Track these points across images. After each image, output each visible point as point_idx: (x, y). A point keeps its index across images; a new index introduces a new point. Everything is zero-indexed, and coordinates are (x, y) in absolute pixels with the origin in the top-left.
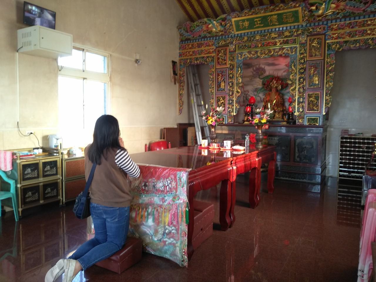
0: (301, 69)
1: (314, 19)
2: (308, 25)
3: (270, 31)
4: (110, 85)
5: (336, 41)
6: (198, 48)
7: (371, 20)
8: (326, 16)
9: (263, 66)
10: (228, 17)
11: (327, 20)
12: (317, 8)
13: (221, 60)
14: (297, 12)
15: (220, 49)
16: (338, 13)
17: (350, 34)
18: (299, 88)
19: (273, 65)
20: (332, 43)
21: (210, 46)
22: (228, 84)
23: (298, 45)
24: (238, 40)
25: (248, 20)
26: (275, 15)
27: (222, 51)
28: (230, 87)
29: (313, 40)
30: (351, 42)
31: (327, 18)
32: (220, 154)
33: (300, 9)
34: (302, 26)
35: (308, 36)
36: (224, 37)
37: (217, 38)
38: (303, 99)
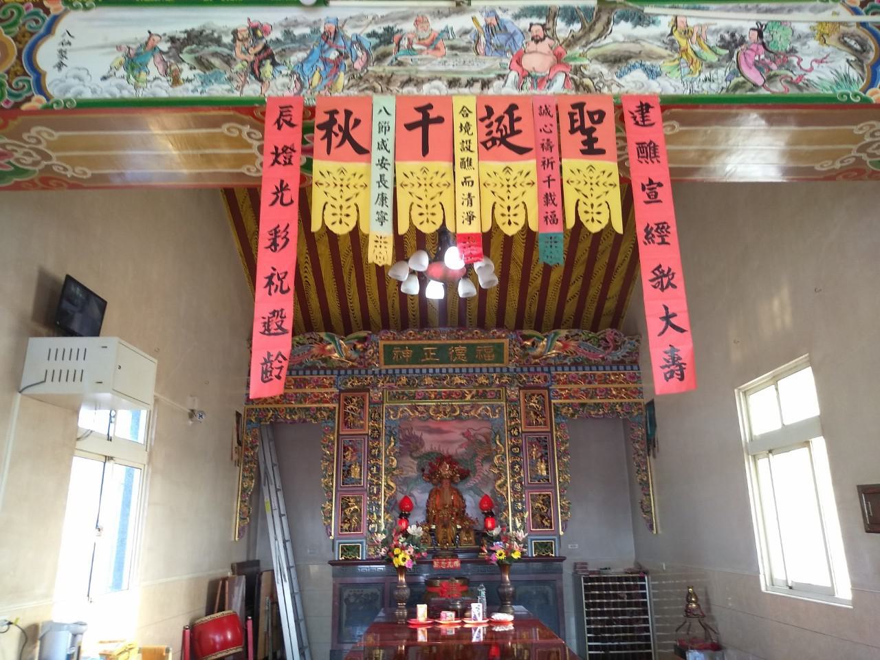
0: (515, 446)
1: (527, 361)
2: (519, 369)
3: (451, 371)
4: (148, 472)
5: (567, 401)
6: (297, 388)
7: (615, 374)
8: (545, 359)
9: (418, 434)
10: (374, 337)
11: (549, 365)
12: (533, 344)
13: (352, 419)
14: (501, 346)
15: (349, 395)
16: (565, 357)
17: (586, 393)
18: (513, 483)
19: (439, 431)
20: (561, 404)
21: (325, 387)
22: (369, 469)
23: (504, 403)
24: (389, 382)
25: (410, 347)
26: (463, 345)
27: (355, 400)
28: (373, 476)
29: (530, 397)
30: (590, 406)
31: (548, 361)
32: (465, 633)
33: (506, 342)
34: (508, 369)
35: (520, 388)
36: (356, 372)
37: (342, 372)
38: (523, 503)
